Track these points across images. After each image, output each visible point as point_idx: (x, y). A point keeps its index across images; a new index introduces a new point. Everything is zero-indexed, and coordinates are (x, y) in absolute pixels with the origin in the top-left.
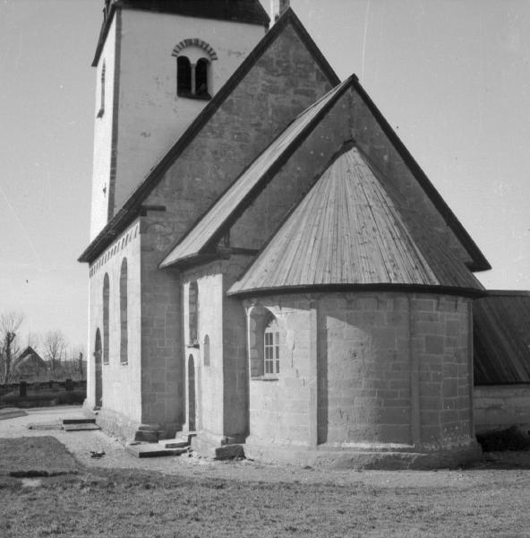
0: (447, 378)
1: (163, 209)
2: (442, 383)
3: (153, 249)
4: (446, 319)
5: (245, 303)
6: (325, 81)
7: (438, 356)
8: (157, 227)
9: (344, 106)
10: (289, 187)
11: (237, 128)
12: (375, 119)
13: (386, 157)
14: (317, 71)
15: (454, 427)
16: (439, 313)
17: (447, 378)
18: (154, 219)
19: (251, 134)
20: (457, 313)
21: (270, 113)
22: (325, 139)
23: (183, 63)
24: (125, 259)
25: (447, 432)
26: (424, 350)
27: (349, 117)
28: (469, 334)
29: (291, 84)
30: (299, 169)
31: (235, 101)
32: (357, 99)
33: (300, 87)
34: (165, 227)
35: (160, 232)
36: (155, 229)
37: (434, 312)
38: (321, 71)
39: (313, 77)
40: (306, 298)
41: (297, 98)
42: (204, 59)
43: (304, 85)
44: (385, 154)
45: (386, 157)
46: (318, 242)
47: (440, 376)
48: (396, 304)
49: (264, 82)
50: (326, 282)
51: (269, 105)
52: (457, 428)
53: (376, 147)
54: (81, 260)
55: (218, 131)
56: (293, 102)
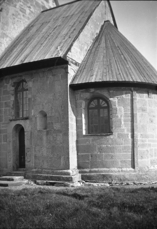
56: (42, 2)
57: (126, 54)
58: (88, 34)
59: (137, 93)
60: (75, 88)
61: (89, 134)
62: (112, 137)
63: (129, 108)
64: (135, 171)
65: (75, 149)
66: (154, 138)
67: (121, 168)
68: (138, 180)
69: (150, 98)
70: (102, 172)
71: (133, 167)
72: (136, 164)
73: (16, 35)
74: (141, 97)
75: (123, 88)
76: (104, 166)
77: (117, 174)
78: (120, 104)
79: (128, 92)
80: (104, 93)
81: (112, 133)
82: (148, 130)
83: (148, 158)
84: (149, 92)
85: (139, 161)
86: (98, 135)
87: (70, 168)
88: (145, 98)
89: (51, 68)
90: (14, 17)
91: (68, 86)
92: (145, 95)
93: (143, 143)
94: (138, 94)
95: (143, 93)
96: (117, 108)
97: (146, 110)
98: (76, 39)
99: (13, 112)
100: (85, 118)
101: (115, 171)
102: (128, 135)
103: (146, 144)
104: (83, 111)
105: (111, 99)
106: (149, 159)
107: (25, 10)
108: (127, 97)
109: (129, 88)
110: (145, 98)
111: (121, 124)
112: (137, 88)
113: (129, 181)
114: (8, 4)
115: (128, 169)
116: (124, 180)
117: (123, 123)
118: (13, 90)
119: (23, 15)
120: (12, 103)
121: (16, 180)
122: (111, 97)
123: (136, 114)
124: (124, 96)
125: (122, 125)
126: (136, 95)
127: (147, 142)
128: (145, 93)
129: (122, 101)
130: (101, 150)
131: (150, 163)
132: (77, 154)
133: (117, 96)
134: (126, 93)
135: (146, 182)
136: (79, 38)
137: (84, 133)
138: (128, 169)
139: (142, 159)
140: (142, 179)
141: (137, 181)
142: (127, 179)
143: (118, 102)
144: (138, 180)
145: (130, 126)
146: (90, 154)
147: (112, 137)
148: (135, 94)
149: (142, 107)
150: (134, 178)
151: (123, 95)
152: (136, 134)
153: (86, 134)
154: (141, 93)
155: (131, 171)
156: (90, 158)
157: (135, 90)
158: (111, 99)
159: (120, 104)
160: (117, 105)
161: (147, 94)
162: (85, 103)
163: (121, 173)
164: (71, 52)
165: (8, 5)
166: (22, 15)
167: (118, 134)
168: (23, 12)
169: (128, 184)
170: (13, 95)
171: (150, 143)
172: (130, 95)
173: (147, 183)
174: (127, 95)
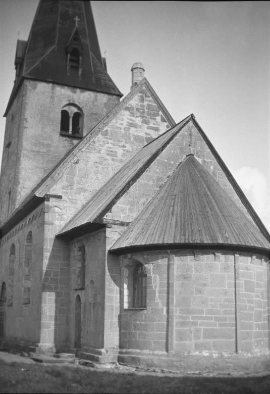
0: (256, 309)
1: (60, 197)
2: (254, 312)
3: (53, 224)
4: (256, 270)
5: (121, 257)
6: (166, 122)
7: (252, 294)
8: (56, 209)
9: (186, 133)
10: (151, 183)
11: (110, 148)
12: (205, 143)
13: (212, 167)
14: (161, 116)
15: (260, 342)
16: (252, 265)
17: (256, 309)
18: (55, 204)
19: (118, 152)
20: (262, 267)
21: (132, 139)
22: (174, 152)
23: (65, 114)
24: (30, 232)
25: (257, 346)
26: (243, 289)
27: (189, 140)
28: (268, 281)
29: (145, 122)
30: (158, 170)
31: (109, 131)
32: (195, 130)
33: (151, 125)
34: (61, 209)
35: (58, 213)
36: (55, 211)
37: (249, 264)
38: (163, 116)
39: (159, 119)
40: (167, 253)
41: (149, 131)
42: (77, 112)
43: (154, 124)
44: (211, 165)
45: (212, 167)
46: (175, 216)
47: (253, 307)
48: (226, 260)
49: (128, 120)
50: (177, 242)
51: (131, 135)
52: (262, 343)
53: (205, 160)
54: (192, 115)
55: (98, 149)
56: (146, 133)
57: (179, 204)
58: (148, 181)
59: (176, 256)
60: (116, 254)
61: (134, 307)
62: (145, 312)
63: (165, 275)
64: (168, 356)
65: (117, 325)
66: (203, 314)
67: (154, 350)
68: (168, 367)
69: (198, 260)
70: (134, 353)
71: (167, 350)
72: (169, 346)
73: (100, 186)
74: (182, 261)
75: (157, 251)
76: (137, 347)
77: (145, 357)
78: (155, 269)
79: (164, 255)
80: (139, 258)
81: (146, 307)
82: (191, 303)
83: (191, 340)
84: (195, 252)
85: (175, 342)
86: (137, 310)
87: (105, 346)
88: (189, 261)
89: (98, 231)
90: (96, 165)
91: (107, 252)
92: (212, 256)
93: (183, 320)
94: (179, 257)
95: (187, 256)
96: (151, 277)
97: (191, 277)
98: (123, 194)
99: (79, 281)
100: (128, 288)
101: (145, 354)
102: (162, 309)
103: (189, 322)
104: (126, 280)
105: (146, 266)
106: (193, 342)
107: (116, 152)
108: (163, 262)
109: (164, 251)
110: (189, 261)
111: (155, 296)
112: (175, 250)
113: (157, 367)
114: (88, 152)
115: (160, 353)
116: (152, 366)
117: (157, 295)
118: (80, 255)
119: (113, 160)
120: (78, 270)
121: (64, 357)
122: (146, 264)
123: (173, 283)
124: (160, 261)
125: (156, 298)
126: (173, 259)
127: (191, 320)
128: (190, 255)
129: (157, 267)
130: (135, 326)
131: (194, 347)
132: (120, 331)
133: (152, 261)
134: (162, 258)
135: (178, 370)
136: (128, 191)
137: (126, 306)
138: (160, 353)
139: (181, 341)
140: (174, 367)
141: (167, 368)
142: (155, 364)
143: (153, 269)
144: (168, 367)
145: (166, 298)
146: (128, 331)
147: (145, 312)
148: (173, 257)
149: (184, 274)
150: (163, 364)
151: (158, 259)
152: (172, 309)
153: (129, 307)
154: (183, 256)
155: (163, 355)
156: (128, 336)
157: (172, 253)
158: (146, 266)
159: (155, 269)
160: (152, 273)
161: (193, 257)
162: (127, 270)
163: (152, 357)
164: (111, 212)
165: (88, 153)
166: (110, 160)
167: (152, 308)
168: (112, 155)
169: (154, 371)
170: (79, 261)
171: (195, 321)
172: (167, 259)
173: (179, 372)
174: (163, 260)
